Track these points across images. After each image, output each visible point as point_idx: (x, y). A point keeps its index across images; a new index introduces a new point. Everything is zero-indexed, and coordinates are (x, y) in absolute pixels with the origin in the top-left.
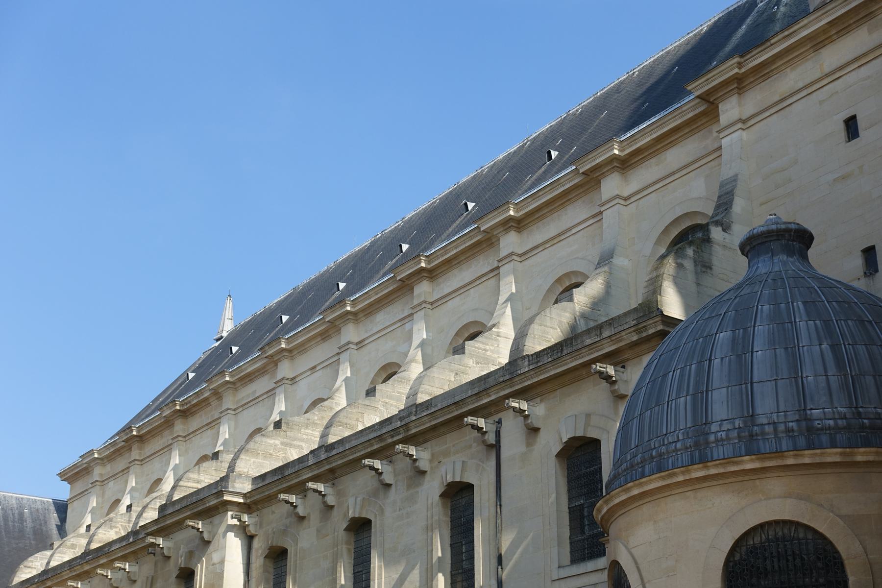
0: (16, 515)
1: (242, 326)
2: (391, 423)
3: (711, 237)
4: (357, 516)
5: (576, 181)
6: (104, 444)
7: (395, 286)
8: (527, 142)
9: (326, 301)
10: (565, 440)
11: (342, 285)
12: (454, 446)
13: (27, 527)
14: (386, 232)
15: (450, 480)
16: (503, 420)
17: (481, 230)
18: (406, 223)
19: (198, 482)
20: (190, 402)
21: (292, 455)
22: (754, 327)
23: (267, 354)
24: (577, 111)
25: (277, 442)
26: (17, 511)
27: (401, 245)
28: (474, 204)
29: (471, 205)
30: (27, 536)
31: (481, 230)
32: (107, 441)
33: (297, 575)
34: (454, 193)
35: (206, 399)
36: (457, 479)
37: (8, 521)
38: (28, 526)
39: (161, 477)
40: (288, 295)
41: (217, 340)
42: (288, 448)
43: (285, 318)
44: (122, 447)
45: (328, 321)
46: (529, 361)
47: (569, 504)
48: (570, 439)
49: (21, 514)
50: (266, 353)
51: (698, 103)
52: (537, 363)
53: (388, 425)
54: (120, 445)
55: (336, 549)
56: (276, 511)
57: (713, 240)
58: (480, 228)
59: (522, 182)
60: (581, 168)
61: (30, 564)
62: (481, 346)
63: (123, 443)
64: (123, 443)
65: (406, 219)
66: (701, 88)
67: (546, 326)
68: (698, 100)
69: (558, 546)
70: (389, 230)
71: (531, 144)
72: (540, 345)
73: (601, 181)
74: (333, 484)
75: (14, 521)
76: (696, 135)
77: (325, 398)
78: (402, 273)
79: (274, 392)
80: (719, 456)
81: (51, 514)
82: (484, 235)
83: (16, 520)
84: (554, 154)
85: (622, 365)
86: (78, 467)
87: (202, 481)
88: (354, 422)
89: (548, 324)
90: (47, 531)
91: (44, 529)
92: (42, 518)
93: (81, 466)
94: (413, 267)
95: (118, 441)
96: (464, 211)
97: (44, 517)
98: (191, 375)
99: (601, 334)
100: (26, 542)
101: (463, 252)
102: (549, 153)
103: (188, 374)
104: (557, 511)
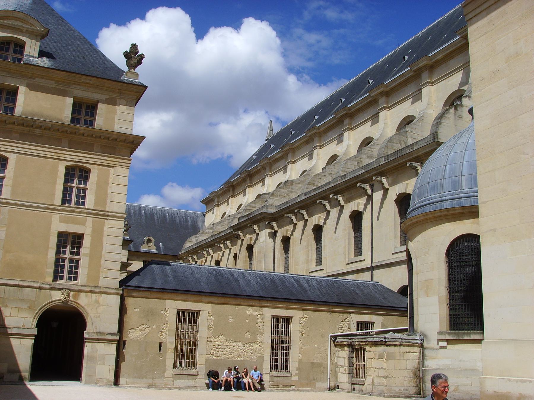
0: (184, 219)
1: (276, 134)
2: (330, 184)
3: (462, 104)
4: (316, 224)
5: (410, 74)
6: (219, 188)
7: (336, 120)
8: (398, 49)
9: (310, 125)
10: (352, 210)
11: (343, 100)
12: (355, 195)
13: (189, 224)
14: (337, 91)
15: (314, 224)
16: (374, 184)
17: (371, 96)
18: (345, 87)
19: (255, 207)
20: (252, 171)
21: (293, 196)
22: (465, 151)
23: (283, 150)
24: (419, 35)
25: (286, 191)
26: (185, 218)
27: (404, 56)
28: (373, 80)
29: (371, 81)
30: (190, 228)
31: (371, 96)
32: (220, 187)
33: (294, 248)
34: (366, 73)
35: (259, 169)
36: (356, 210)
37: (181, 222)
38: (190, 224)
39: (242, 203)
40: (296, 120)
41: (266, 140)
42: (291, 193)
43: (293, 132)
44: (226, 190)
45: (308, 136)
46: (385, 159)
47: (400, 221)
48: (399, 194)
49: (186, 219)
50: (283, 150)
51: (462, 40)
52: (388, 160)
53: (329, 185)
54: (225, 189)
55: (308, 238)
56: (285, 221)
57: (463, 105)
58: (370, 95)
59: (392, 71)
60: (412, 69)
61: (190, 240)
62: (370, 149)
63: (226, 188)
64: (226, 188)
65: (346, 85)
66: (462, 33)
67: (393, 143)
68: (462, 39)
69: (395, 239)
70: (338, 90)
71: (447, 17)
72: (390, 151)
73: (422, 74)
74: (307, 210)
75: (183, 222)
76: (462, 54)
77: (257, 199)
78: (338, 115)
79: (287, 167)
80: (255, 269)
81: (199, 219)
82: (413, 73)
83: (185, 221)
84: (407, 58)
85: (421, 162)
86: (209, 198)
87: (256, 207)
88: (316, 183)
89: (394, 142)
90: (197, 226)
91: (196, 225)
92: (195, 220)
93: (210, 198)
94: (342, 113)
95: (224, 187)
96: (341, 102)
97: (196, 219)
98: (255, 157)
99: (413, 148)
100: (189, 230)
101: (364, 105)
102: (404, 58)
103: (253, 157)
104: (395, 224)
